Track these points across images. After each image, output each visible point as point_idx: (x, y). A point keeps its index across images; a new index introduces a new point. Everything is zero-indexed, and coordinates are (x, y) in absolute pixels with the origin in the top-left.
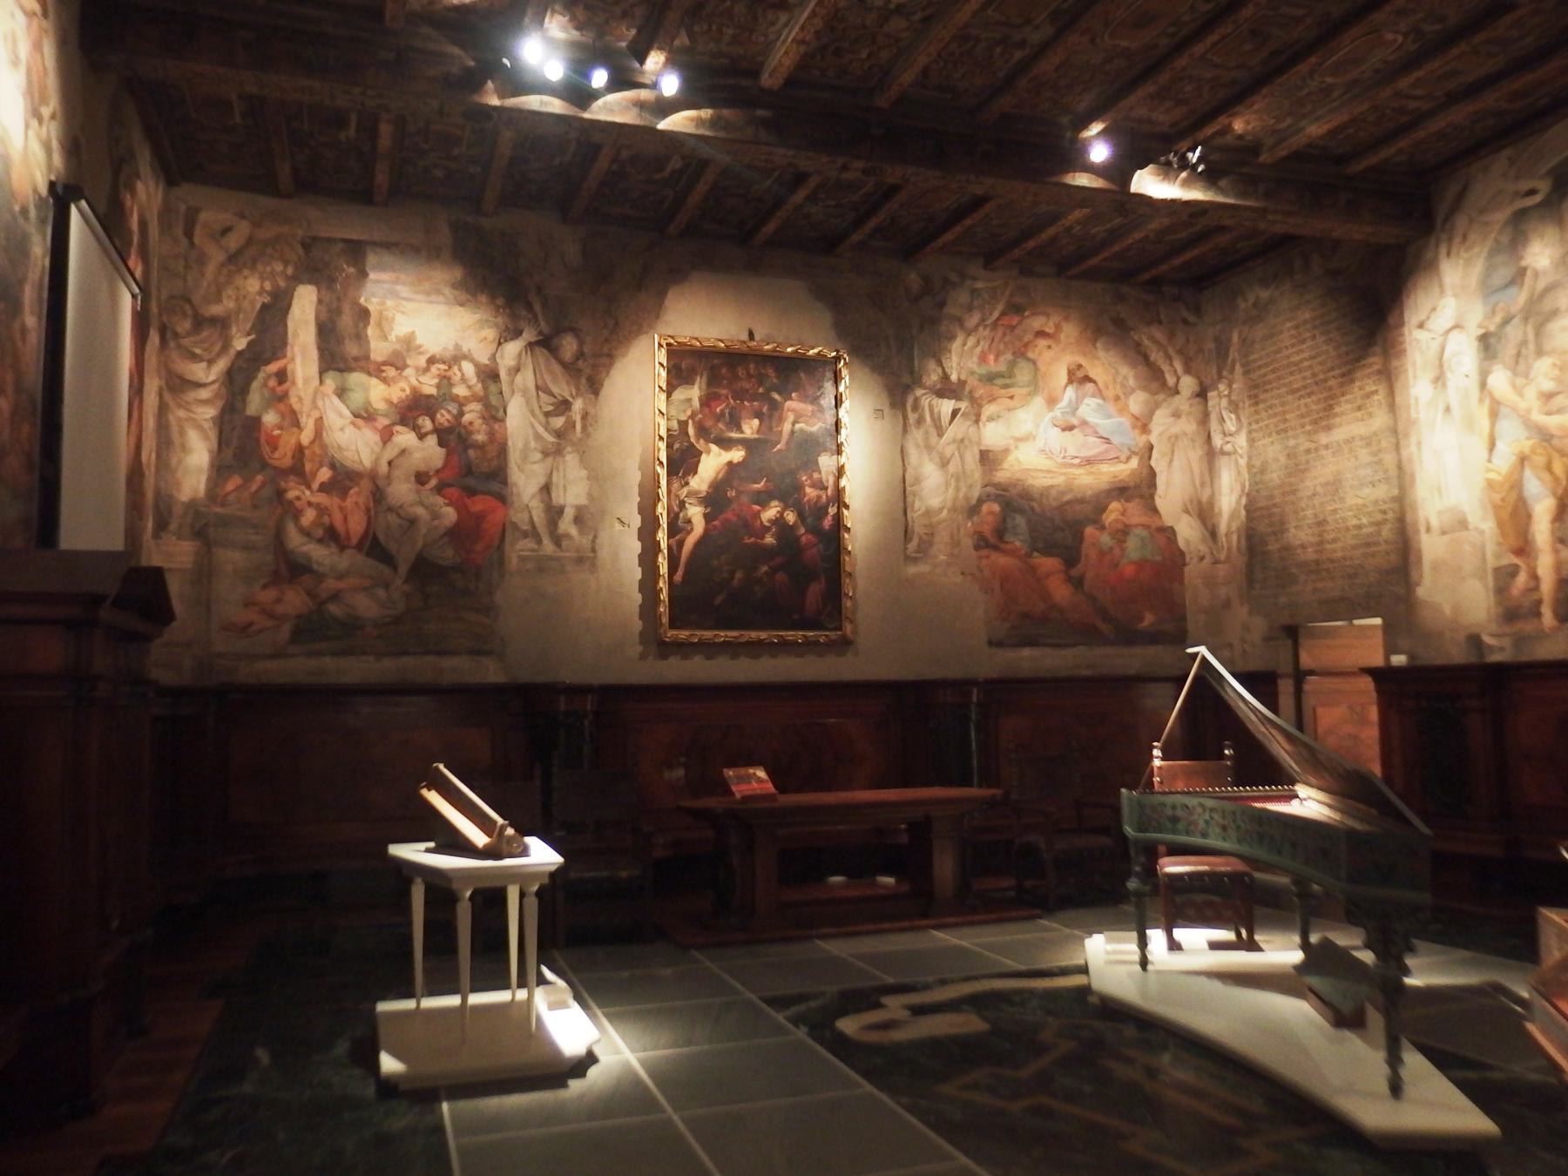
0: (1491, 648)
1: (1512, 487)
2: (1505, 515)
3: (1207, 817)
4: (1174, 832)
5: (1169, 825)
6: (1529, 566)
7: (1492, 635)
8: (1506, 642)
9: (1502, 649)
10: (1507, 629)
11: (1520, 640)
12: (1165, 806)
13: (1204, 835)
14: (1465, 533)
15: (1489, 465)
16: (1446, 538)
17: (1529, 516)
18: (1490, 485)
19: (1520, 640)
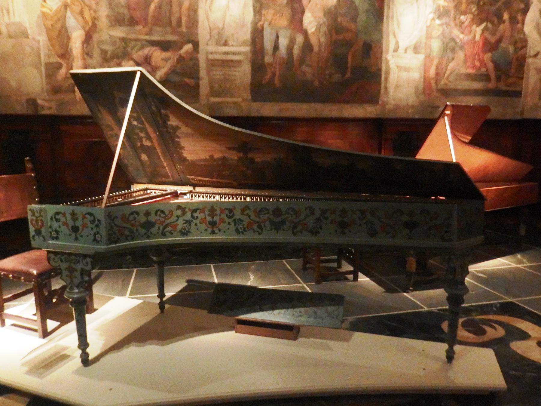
0: (43, 107)
1: (58, 20)
2: (54, 34)
3: (188, 216)
4: (148, 237)
5: (143, 231)
6: (68, 64)
7: (44, 100)
8: (53, 104)
9: (50, 108)
10: (53, 97)
11: (60, 104)
12: (138, 213)
13: (184, 233)
14: (25, 40)
15: (44, 4)
16: (12, 41)
17: (69, 38)
18: (44, 15)
19: (60, 104)
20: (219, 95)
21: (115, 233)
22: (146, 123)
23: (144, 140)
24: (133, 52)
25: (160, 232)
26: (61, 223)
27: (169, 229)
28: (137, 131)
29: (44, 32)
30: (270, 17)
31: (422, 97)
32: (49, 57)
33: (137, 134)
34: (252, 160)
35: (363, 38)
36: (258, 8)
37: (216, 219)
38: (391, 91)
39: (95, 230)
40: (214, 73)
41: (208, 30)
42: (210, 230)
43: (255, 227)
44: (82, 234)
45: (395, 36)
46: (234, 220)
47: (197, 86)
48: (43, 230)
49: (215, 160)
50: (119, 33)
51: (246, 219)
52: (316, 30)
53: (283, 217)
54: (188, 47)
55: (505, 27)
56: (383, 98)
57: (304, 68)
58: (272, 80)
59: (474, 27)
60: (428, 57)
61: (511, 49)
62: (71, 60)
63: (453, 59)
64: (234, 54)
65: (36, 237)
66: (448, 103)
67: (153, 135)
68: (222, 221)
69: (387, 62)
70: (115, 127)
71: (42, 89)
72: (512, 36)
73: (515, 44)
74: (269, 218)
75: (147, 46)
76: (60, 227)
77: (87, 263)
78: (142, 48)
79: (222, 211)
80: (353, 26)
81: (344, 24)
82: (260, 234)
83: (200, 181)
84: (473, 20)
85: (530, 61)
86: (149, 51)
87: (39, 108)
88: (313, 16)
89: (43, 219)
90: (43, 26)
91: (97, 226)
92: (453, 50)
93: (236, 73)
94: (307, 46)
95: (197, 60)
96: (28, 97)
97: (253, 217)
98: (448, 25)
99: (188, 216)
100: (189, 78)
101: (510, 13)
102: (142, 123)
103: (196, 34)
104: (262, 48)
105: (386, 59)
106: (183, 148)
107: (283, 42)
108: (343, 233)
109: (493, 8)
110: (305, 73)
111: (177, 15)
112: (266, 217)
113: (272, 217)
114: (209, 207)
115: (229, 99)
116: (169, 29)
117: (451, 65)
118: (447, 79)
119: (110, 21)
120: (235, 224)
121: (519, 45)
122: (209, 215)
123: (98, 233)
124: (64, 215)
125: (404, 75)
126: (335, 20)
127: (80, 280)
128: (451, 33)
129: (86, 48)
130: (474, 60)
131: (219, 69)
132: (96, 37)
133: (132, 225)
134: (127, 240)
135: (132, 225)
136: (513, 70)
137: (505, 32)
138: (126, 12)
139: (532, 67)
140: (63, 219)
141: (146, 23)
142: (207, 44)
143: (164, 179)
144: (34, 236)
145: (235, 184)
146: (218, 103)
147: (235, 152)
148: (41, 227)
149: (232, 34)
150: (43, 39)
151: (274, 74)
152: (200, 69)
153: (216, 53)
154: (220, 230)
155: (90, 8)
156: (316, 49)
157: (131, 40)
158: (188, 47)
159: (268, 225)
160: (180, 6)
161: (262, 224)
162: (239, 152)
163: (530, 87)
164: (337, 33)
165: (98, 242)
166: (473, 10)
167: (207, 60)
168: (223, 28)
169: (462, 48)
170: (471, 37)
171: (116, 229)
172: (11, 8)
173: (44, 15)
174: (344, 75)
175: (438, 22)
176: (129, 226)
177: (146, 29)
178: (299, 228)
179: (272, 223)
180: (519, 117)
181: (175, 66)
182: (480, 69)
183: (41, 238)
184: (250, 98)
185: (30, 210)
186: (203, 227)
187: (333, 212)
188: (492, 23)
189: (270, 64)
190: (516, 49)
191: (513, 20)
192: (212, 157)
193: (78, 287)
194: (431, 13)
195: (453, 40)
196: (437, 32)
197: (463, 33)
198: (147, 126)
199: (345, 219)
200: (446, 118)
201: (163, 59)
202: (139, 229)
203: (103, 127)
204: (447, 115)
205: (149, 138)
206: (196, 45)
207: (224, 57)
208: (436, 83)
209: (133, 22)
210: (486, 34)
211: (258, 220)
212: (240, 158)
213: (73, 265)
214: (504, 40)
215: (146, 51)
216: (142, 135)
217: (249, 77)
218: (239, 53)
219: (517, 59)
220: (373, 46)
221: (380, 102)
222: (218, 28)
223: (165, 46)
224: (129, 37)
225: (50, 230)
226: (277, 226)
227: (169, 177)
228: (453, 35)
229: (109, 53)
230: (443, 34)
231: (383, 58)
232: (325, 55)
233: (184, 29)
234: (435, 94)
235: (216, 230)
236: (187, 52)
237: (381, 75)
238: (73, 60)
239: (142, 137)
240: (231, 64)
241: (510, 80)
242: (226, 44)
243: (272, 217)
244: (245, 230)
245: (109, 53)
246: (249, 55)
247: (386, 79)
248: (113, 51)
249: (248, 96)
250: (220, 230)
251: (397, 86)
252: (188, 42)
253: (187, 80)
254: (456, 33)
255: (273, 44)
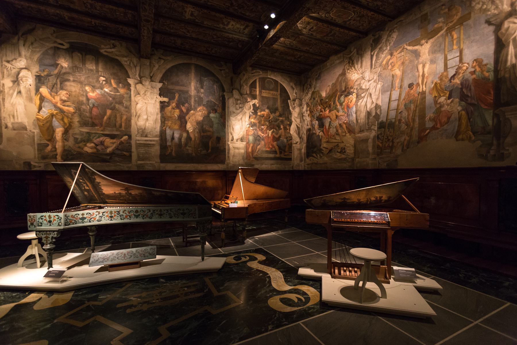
0: (35, 166)
1: (47, 122)
3: (101, 215)
4: (83, 223)
8: (42, 165)
20: (143, 160)
21: (68, 222)
22: (86, 181)
23: (85, 187)
24: (94, 139)
25: (88, 221)
26: (43, 220)
27: (93, 219)
28: (82, 184)
29: (38, 127)
30: (169, 124)
31: (246, 161)
32: (40, 140)
33: (83, 185)
34: (131, 194)
35: (216, 135)
36: (163, 120)
37: (113, 215)
38: (231, 158)
39: (59, 221)
40: (140, 149)
41: (137, 130)
42: (110, 219)
43: (128, 217)
44: (53, 223)
45: (232, 134)
46: (120, 215)
47: (131, 156)
48: (35, 223)
49: (116, 194)
50: (85, 130)
51: (125, 215)
52: (193, 131)
53: (139, 213)
54: (126, 137)
55: (282, 131)
56: (227, 161)
57: (187, 148)
58: (171, 153)
59: (268, 131)
60: (248, 143)
61: (285, 140)
62: (55, 142)
63: (259, 144)
64: (151, 141)
65: (31, 226)
66: (240, 167)
67: (89, 185)
68: (115, 215)
69: (229, 145)
70: (72, 182)
71: (35, 156)
72: (285, 135)
73: (287, 138)
74: (133, 214)
75: (102, 137)
76: (43, 221)
77: (55, 234)
78: (99, 137)
79: (115, 212)
80: (211, 129)
81: (207, 128)
82: (130, 220)
83: (112, 202)
84: (267, 128)
85: (294, 145)
86: (103, 139)
87: (32, 166)
88: (191, 125)
89: (35, 219)
90: (37, 125)
91: (60, 220)
92: (259, 140)
93: (152, 150)
94: (189, 138)
95: (130, 143)
96: (24, 161)
97: (127, 214)
98: (256, 130)
99: (101, 215)
100: (126, 152)
101: (283, 126)
102: (84, 181)
103: (130, 132)
104: (166, 139)
105: (228, 144)
106: (103, 190)
107: (177, 135)
108: (161, 218)
109: (276, 123)
110: (188, 150)
111: (119, 122)
112: (132, 213)
113: (134, 213)
114: (110, 211)
115: (148, 162)
116: (114, 129)
117: (258, 147)
118: (257, 152)
119: (80, 124)
120: (120, 216)
121: (289, 139)
122: (110, 214)
123: (60, 222)
124: (45, 217)
125: (237, 151)
126: (202, 126)
127: (51, 241)
128: (258, 133)
129: (65, 137)
130: (269, 145)
131: (143, 148)
132: (71, 132)
133: (76, 219)
134: (73, 224)
135: (77, 219)
136: (287, 149)
137: (282, 133)
138: (90, 120)
139: (295, 148)
140: (45, 218)
141: (101, 125)
142: (136, 136)
143: (95, 202)
144: (30, 226)
145: (126, 202)
146: (142, 164)
147: (124, 191)
148: (34, 222)
149: (150, 132)
150: (36, 131)
151: (172, 150)
152: (132, 148)
153: (141, 140)
154: (114, 219)
155: (68, 117)
156: (193, 139)
157: (92, 133)
158: (126, 137)
159: (133, 216)
160: (121, 118)
161: (131, 216)
162: (125, 191)
163: (295, 156)
164: (203, 132)
165: (60, 226)
166: (267, 124)
167: (136, 143)
168: (145, 129)
169: (263, 140)
170: (267, 135)
171: (68, 220)
172: (15, 114)
173: (38, 119)
174: (207, 151)
175: (251, 128)
176: (74, 219)
177: (102, 128)
178: (145, 216)
179: (135, 215)
180: (291, 169)
181: (118, 146)
182: (272, 149)
183: (33, 226)
184: (160, 161)
185: (29, 216)
186: (107, 218)
187: (157, 211)
188: (276, 129)
189: (170, 146)
190: (287, 140)
191: (285, 128)
192: (115, 193)
193: (49, 244)
194: (248, 125)
195: (259, 136)
196: (251, 133)
197: (263, 133)
198: (87, 182)
199: (162, 213)
200: (240, 173)
201: (111, 143)
202: (79, 220)
203: (67, 182)
204: (240, 172)
205: (88, 186)
206: (130, 137)
207: (145, 142)
208: (252, 154)
209: (93, 125)
210: (274, 134)
211: (129, 215)
212: (126, 193)
213: (48, 235)
214: (282, 136)
215: (101, 139)
216: (84, 185)
217: (159, 152)
218: (154, 141)
219: (288, 144)
220: (221, 138)
221: (226, 163)
222: (142, 129)
223: (112, 137)
224: (91, 132)
225: (38, 223)
226: (137, 217)
227: (98, 201)
228: (259, 134)
229: (79, 139)
230: (254, 134)
231: (227, 144)
232: (198, 142)
233: (123, 129)
234: (252, 159)
235: (113, 219)
236: (125, 140)
237: (225, 151)
238: (56, 143)
239: (85, 186)
240: (149, 145)
241: (286, 153)
242: (146, 136)
243: (134, 213)
244: (124, 218)
245: (79, 139)
246: (159, 141)
247: (228, 153)
248: (82, 138)
249: (159, 160)
250: (114, 219)
251: (234, 156)
252: (126, 135)
253: (124, 153)
254: (260, 133)
255: (171, 137)
